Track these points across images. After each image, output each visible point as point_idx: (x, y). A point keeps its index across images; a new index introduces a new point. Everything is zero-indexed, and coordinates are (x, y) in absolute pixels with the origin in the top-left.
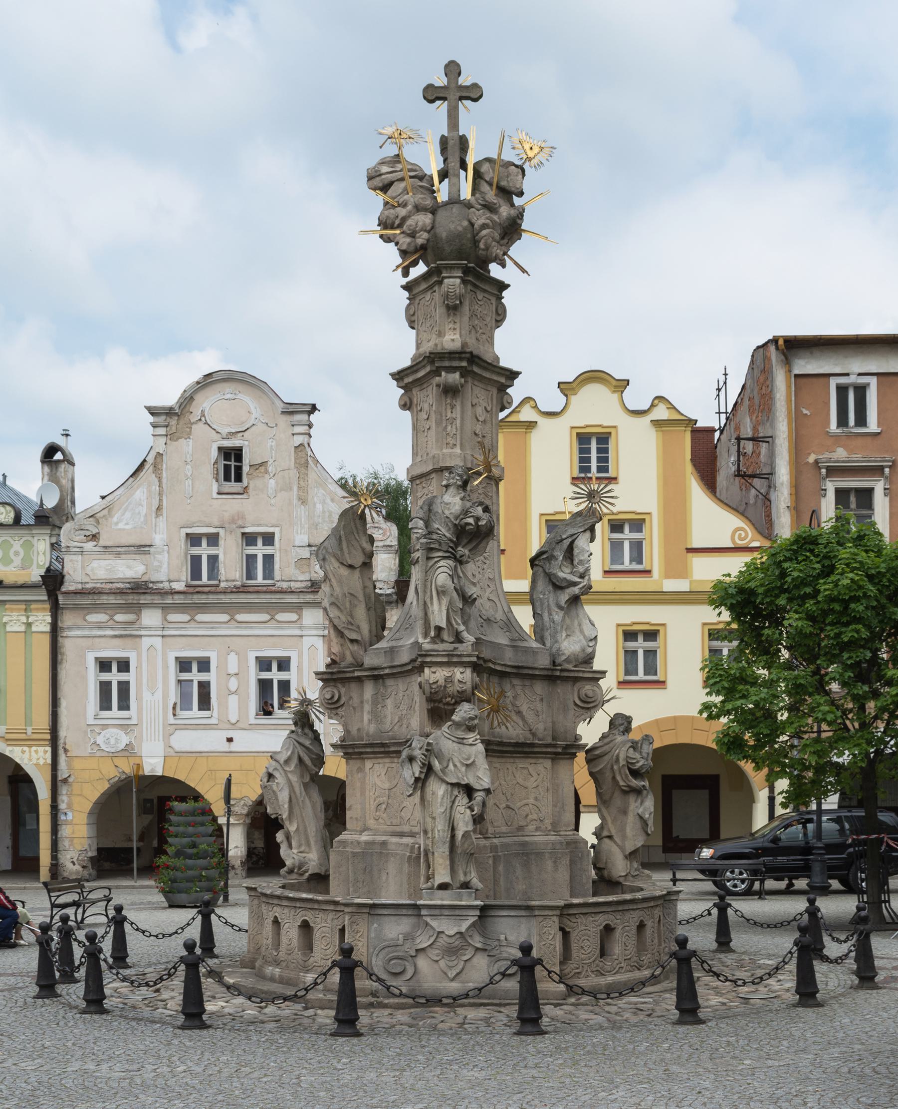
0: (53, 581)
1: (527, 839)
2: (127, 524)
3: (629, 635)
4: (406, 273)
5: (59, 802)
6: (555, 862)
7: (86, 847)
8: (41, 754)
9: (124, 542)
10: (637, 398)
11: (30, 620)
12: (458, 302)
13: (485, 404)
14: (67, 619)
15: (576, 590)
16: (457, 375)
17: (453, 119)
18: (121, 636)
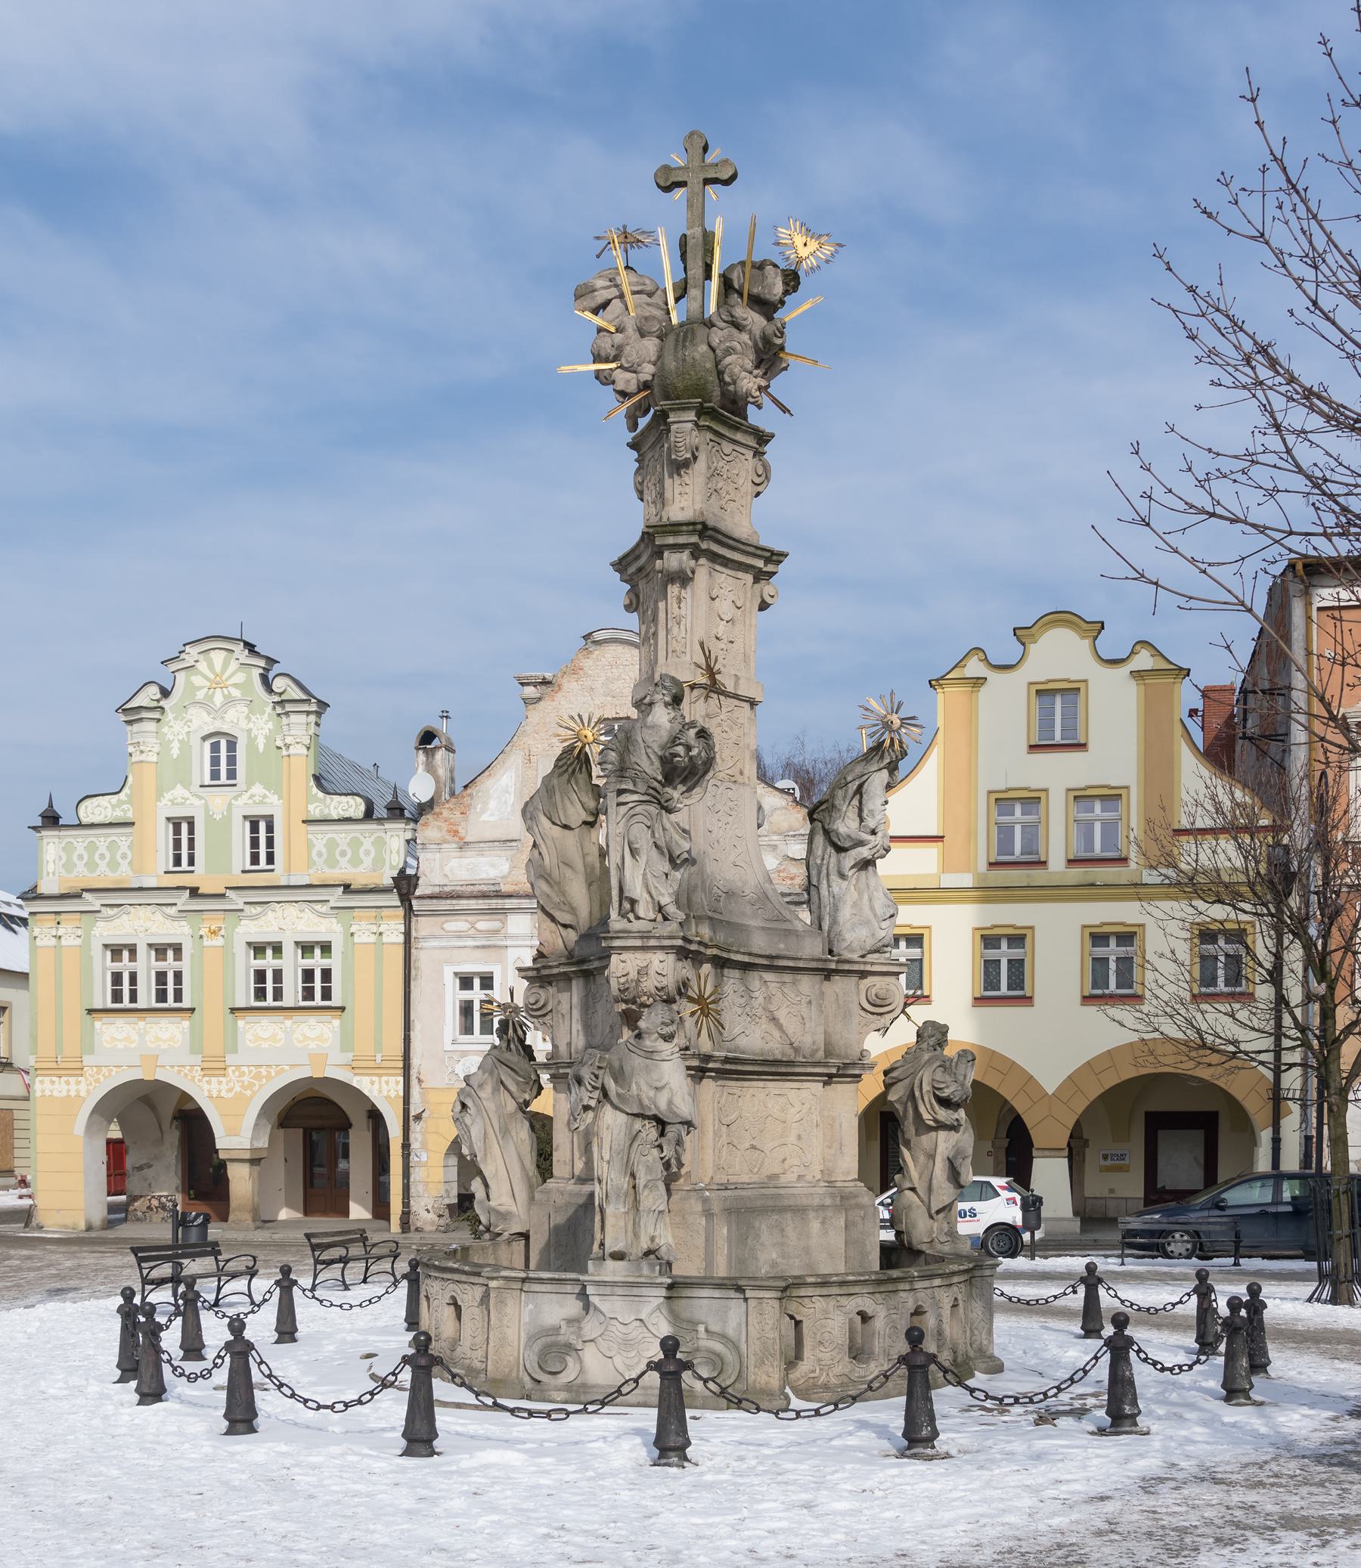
0: (405, 885)
1: (782, 1191)
2: (492, 815)
3: (1099, 938)
4: (633, 426)
5: (412, 1140)
6: (823, 1223)
7: (443, 1193)
8: (392, 1085)
9: (488, 836)
10: (1111, 643)
11: (381, 929)
12: (689, 455)
13: (731, 596)
14: (422, 926)
15: (864, 852)
16: (685, 555)
17: (697, 210)
18: (484, 947)
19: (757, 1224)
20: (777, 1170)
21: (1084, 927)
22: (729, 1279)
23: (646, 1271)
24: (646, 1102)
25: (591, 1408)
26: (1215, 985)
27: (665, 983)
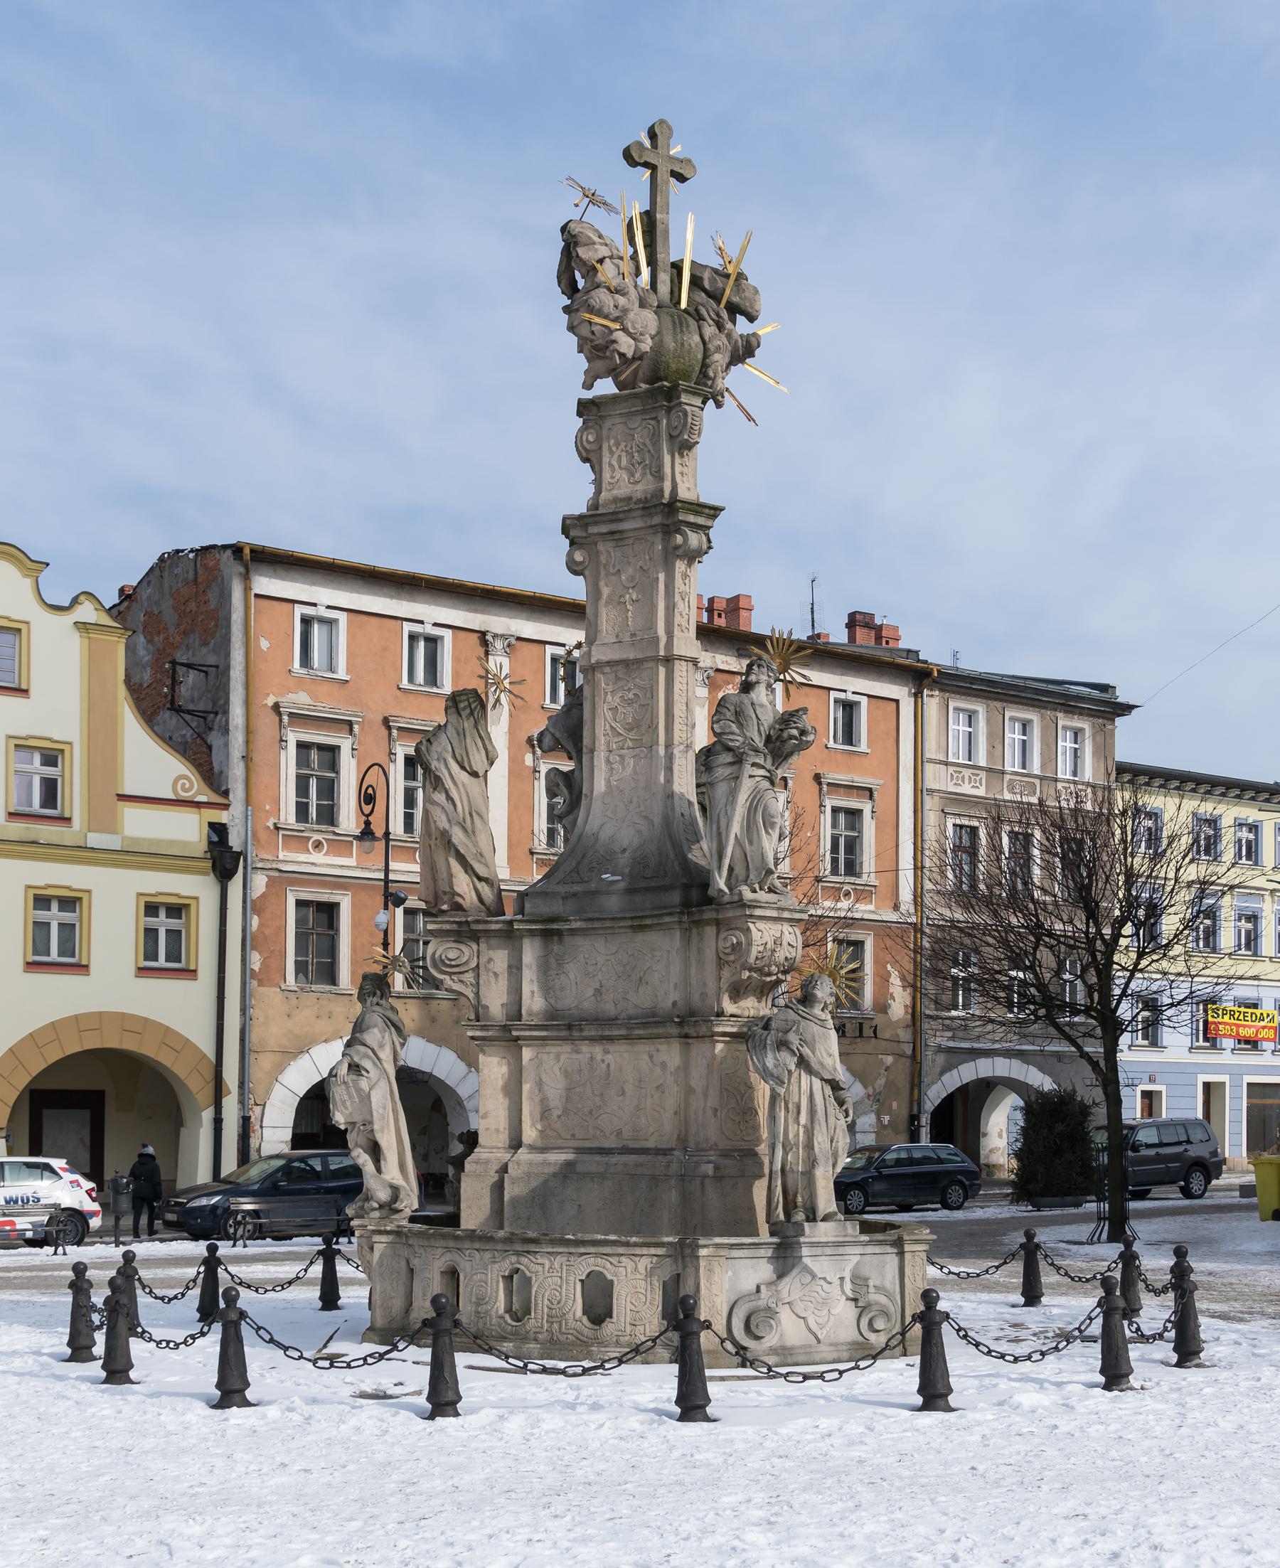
3: (42, 901)
4: (588, 386)
21: (28, 887)
23: (850, 1231)
25: (862, 1364)
26: (156, 959)
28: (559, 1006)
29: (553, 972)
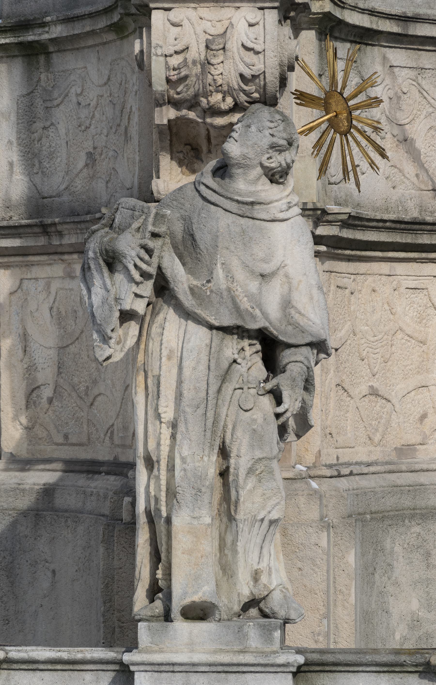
1: (423, 478)
19: (388, 544)
20: (412, 437)
22: (411, 652)
24: (245, 304)
27: (259, 67)
28: (46, 190)
29: (39, 125)
